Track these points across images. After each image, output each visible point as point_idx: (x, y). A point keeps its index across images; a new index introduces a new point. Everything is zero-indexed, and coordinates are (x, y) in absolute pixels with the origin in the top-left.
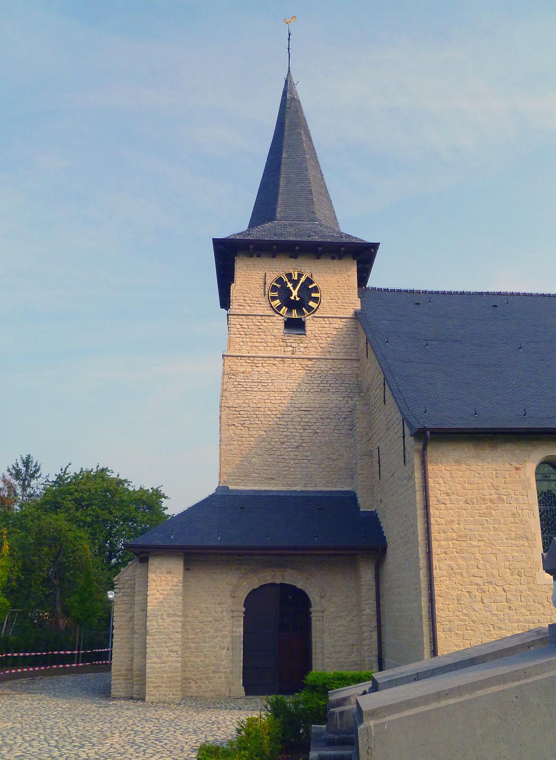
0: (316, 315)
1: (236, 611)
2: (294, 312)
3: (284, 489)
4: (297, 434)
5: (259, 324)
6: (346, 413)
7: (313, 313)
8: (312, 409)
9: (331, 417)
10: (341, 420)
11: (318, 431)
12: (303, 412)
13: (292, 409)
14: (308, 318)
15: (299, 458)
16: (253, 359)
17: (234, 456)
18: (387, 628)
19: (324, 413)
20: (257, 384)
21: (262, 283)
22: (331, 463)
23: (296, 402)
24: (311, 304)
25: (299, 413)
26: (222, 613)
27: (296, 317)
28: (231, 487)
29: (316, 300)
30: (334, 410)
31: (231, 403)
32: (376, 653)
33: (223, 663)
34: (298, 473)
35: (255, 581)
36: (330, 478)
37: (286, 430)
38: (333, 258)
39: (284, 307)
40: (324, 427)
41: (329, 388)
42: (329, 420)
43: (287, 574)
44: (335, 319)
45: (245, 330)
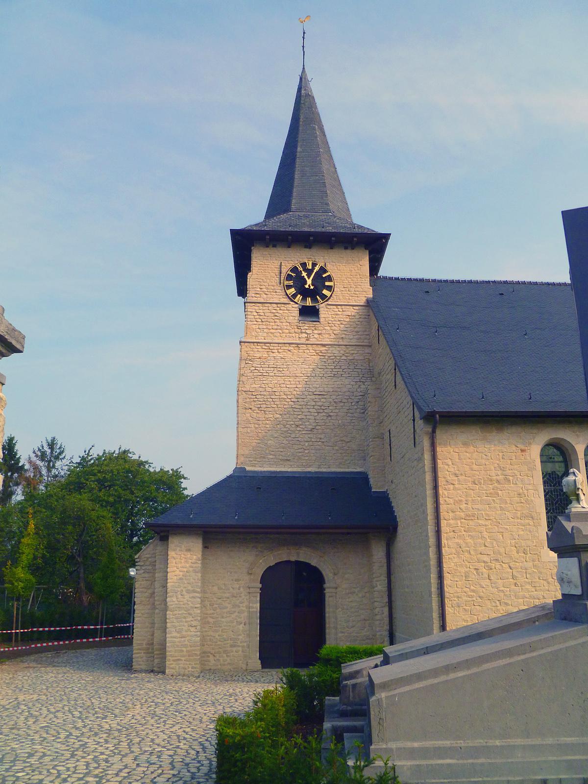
0: (330, 303)
1: (252, 588)
2: (309, 300)
3: (299, 470)
4: (311, 417)
5: (275, 311)
6: (358, 397)
7: (326, 301)
8: (326, 393)
9: (344, 401)
10: (353, 404)
11: (331, 414)
12: (317, 397)
13: (306, 393)
14: (322, 305)
15: (313, 440)
16: (268, 345)
17: (251, 438)
18: (398, 604)
19: (337, 397)
20: (272, 369)
21: (277, 272)
22: (344, 445)
23: (311, 386)
24: (325, 292)
25: (313, 397)
26: (239, 589)
27: (311, 305)
28: (248, 468)
29: (329, 288)
30: (347, 394)
31: (247, 387)
32: (387, 627)
33: (240, 637)
34: (312, 455)
35: (271, 559)
36: (343, 459)
37: (301, 413)
38: (346, 248)
39: (299, 296)
40: (337, 411)
41: (341, 373)
42: (342, 404)
43: (301, 551)
44: (348, 307)
45: (261, 317)
